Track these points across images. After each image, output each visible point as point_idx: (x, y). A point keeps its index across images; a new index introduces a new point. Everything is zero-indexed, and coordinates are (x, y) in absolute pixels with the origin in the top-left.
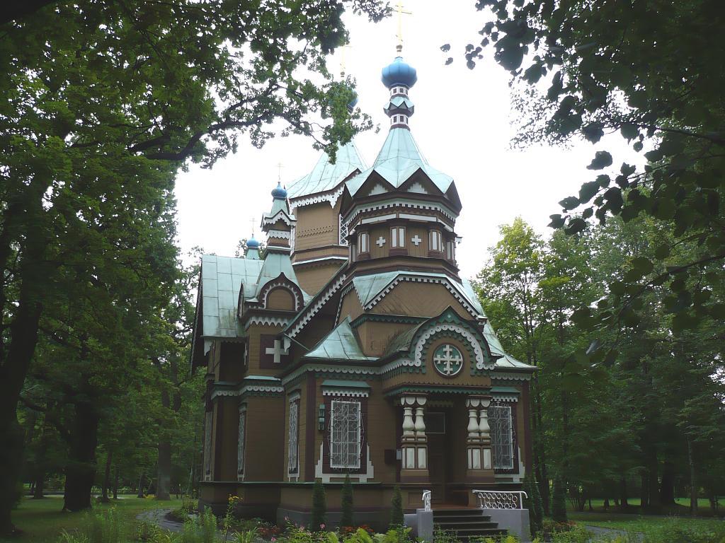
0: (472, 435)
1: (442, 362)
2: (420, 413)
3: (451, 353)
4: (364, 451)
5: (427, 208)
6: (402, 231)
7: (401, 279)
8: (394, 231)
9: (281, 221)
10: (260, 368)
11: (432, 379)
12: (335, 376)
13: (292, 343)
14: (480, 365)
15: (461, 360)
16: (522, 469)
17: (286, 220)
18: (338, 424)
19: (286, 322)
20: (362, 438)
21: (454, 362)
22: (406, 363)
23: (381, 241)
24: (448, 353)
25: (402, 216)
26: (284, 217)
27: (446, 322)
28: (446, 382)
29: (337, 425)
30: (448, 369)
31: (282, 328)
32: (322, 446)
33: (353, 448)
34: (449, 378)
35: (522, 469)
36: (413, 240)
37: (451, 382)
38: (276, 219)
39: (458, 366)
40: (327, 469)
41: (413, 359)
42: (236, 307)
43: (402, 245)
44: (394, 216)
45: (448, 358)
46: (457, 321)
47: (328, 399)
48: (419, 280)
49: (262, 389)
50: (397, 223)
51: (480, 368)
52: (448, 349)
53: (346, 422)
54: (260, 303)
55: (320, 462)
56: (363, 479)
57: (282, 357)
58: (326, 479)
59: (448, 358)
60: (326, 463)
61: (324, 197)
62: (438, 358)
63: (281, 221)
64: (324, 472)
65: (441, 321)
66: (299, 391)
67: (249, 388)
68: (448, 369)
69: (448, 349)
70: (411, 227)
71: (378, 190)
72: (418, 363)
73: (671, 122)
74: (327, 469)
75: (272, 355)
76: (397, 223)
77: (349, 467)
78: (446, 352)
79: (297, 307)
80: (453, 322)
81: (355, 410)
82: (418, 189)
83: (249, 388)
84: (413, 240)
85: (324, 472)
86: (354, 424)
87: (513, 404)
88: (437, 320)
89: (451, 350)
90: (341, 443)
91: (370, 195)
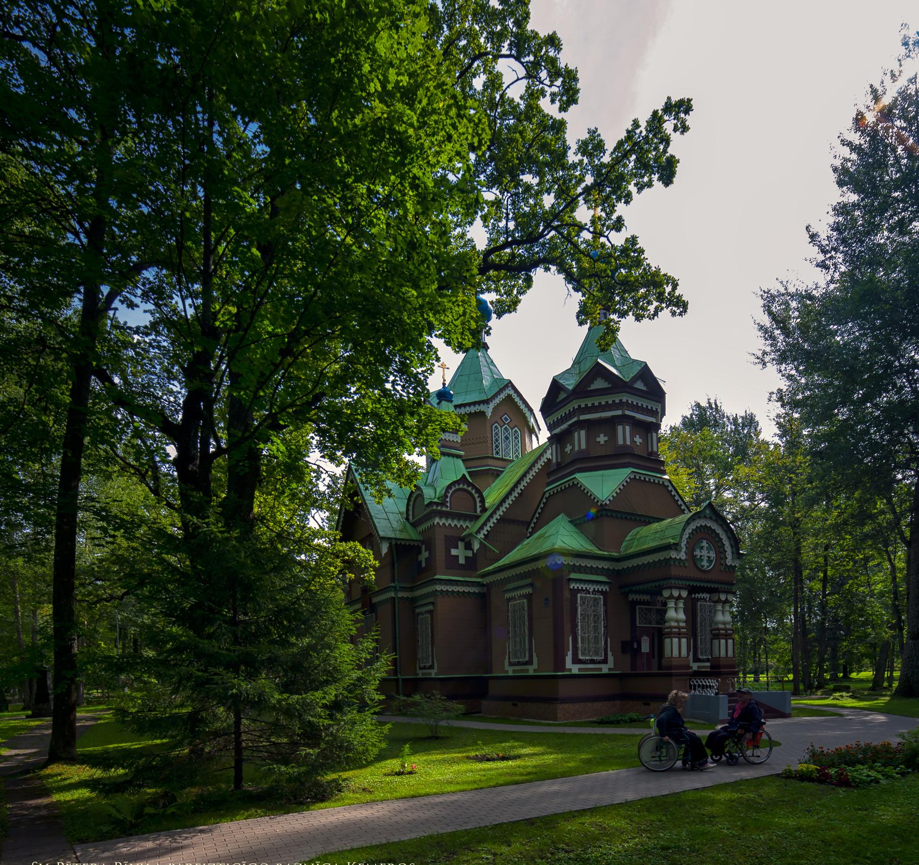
2: (681, 605)
4: (606, 643)
5: (590, 405)
7: (632, 477)
8: (620, 428)
10: (447, 568)
13: (481, 544)
16: (611, 659)
22: (673, 554)
23: (602, 439)
24: (705, 548)
25: (582, 417)
27: (705, 517)
29: (584, 618)
31: (465, 530)
33: (597, 639)
34: (705, 572)
35: (611, 659)
36: (598, 440)
40: (576, 661)
42: (404, 509)
43: (583, 446)
44: (619, 413)
45: (705, 553)
46: (714, 518)
47: (575, 592)
49: (450, 588)
50: (623, 419)
51: (729, 564)
54: (443, 504)
55: (570, 653)
56: (605, 669)
58: (575, 669)
59: (705, 553)
60: (575, 654)
61: (477, 406)
64: (694, 661)
67: (438, 588)
68: (705, 563)
69: (704, 544)
70: (589, 425)
71: (599, 384)
72: (682, 556)
73: (207, 371)
74: (576, 661)
75: (457, 556)
76: (623, 419)
77: (595, 658)
79: (479, 510)
80: (711, 518)
82: (599, 384)
83: (438, 588)
84: (598, 440)
85: (694, 661)
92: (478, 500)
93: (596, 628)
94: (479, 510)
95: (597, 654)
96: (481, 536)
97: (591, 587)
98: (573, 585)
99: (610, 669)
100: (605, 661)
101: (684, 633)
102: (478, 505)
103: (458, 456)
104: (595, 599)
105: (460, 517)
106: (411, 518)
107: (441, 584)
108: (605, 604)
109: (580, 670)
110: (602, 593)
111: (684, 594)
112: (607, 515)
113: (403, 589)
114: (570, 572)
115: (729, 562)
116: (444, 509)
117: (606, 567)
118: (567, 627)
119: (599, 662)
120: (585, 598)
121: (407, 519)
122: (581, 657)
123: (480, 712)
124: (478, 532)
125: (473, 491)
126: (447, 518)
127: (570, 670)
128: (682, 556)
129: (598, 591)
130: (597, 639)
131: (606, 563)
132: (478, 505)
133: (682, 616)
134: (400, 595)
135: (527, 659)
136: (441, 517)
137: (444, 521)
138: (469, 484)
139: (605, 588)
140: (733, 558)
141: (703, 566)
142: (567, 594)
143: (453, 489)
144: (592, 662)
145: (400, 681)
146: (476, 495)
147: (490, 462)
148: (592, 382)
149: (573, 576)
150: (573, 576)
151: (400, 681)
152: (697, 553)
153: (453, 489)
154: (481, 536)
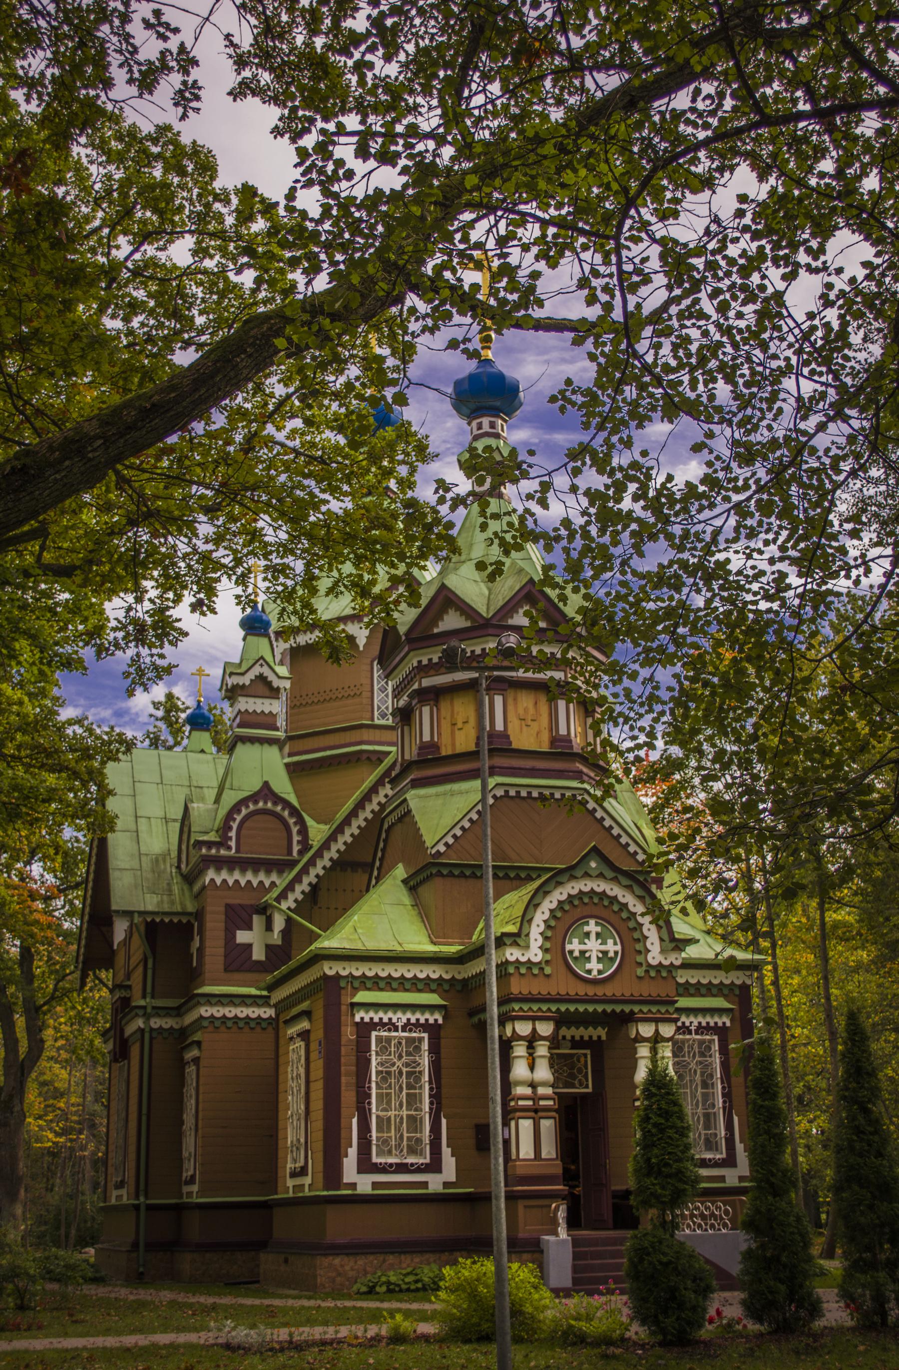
0: (520, 1090)
1: (583, 953)
2: (542, 1050)
3: (598, 935)
6: (426, 710)
9: (261, 678)
11: (564, 986)
12: (376, 983)
14: (655, 955)
15: (618, 948)
16: (449, 1162)
17: (271, 677)
18: (385, 1076)
19: (274, 877)
20: (431, 1103)
21: (605, 953)
24: (593, 936)
25: (426, 682)
26: (266, 671)
27: (587, 875)
28: (591, 991)
30: (594, 966)
32: (355, 1121)
33: (414, 1123)
34: (595, 982)
35: (449, 1162)
37: (600, 991)
38: (251, 675)
39: (612, 960)
41: (527, 947)
45: (593, 946)
46: (609, 874)
47: (365, 1028)
48: (524, 794)
51: (654, 962)
52: (592, 927)
53: (401, 1073)
54: (223, 843)
55: (353, 1152)
56: (435, 1183)
57: (269, 948)
58: (365, 1184)
59: (593, 946)
62: (574, 946)
63: (261, 678)
64: (360, 1171)
65: (579, 873)
66: (307, 1014)
68: (594, 966)
69: (592, 927)
71: (452, 621)
72: (535, 953)
74: (365, 1166)
75: (250, 946)
77: (410, 1160)
78: (587, 935)
79: (296, 848)
80: (601, 876)
81: (418, 1049)
82: (452, 621)
85: (360, 1171)
86: (414, 1076)
87: (721, 1032)
88: (570, 872)
89: (599, 929)
90: (392, 1113)
91: (436, 631)
92: (295, 830)
93: (413, 1100)
94: (296, 848)
95: (412, 1151)
96: (288, 903)
97: (401, 1018)
98: (360, 1015)
99: (446, 1185)
100: (435, 1166)
101: (547, 1109)
102: (296, 838)
103: (271, 741)
104: (410, 1041)
105: (256, 865)
106: (183, 866)
107: (211, 1004)
108: (434, 1049)
109: (375, 1185)
110: (426, 1027)
111: (545, 1029)
112: (440, 874)
113: (159, 1011)
114: (356, 990)
115: (655, 955)
116: (223, 852)
117: (434, 976)
118: (348, 1097)
119: (419, 1169)
120: (389, 1040)
121: (178, 867)
122: (375, 1159)
123: (258, 1282)
124: (283, 896)
125: (286, 813)
126: (231, 870)
127: (353, 1186)
128: (535, 953)
129: (417, 1024)
130: (414, 1123)
131: (434, 967)
132: (296, 838)
133: (543, 1073)
134: (156, 1023)
135: (375, 1159)
136: (218, 870)
137: (224, 875)
138: (278, 799)
139: (437, 1017)
140: (663, 951)
141: (589, 972)
142: (349, 1034)
143: (244, 811)
144: (402, 1168)
145: (143, 1209)
146: (291, 821)
147: (366, 735)
148: (439, 617)
149: (362, 997)
150: (362, 997)
151: (143, 1209)
152: (574, 946)
153: (244, 811)
154: (288, 903)
